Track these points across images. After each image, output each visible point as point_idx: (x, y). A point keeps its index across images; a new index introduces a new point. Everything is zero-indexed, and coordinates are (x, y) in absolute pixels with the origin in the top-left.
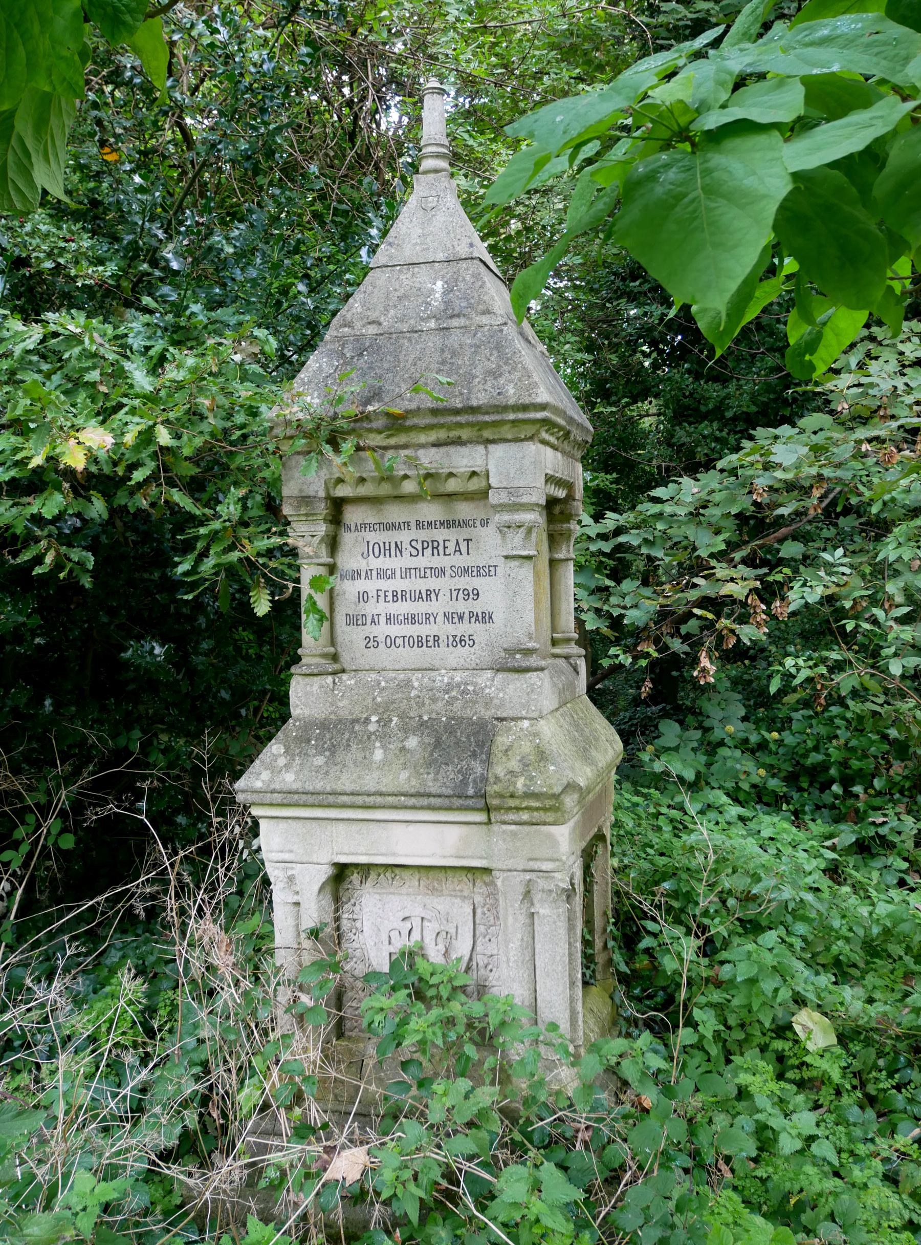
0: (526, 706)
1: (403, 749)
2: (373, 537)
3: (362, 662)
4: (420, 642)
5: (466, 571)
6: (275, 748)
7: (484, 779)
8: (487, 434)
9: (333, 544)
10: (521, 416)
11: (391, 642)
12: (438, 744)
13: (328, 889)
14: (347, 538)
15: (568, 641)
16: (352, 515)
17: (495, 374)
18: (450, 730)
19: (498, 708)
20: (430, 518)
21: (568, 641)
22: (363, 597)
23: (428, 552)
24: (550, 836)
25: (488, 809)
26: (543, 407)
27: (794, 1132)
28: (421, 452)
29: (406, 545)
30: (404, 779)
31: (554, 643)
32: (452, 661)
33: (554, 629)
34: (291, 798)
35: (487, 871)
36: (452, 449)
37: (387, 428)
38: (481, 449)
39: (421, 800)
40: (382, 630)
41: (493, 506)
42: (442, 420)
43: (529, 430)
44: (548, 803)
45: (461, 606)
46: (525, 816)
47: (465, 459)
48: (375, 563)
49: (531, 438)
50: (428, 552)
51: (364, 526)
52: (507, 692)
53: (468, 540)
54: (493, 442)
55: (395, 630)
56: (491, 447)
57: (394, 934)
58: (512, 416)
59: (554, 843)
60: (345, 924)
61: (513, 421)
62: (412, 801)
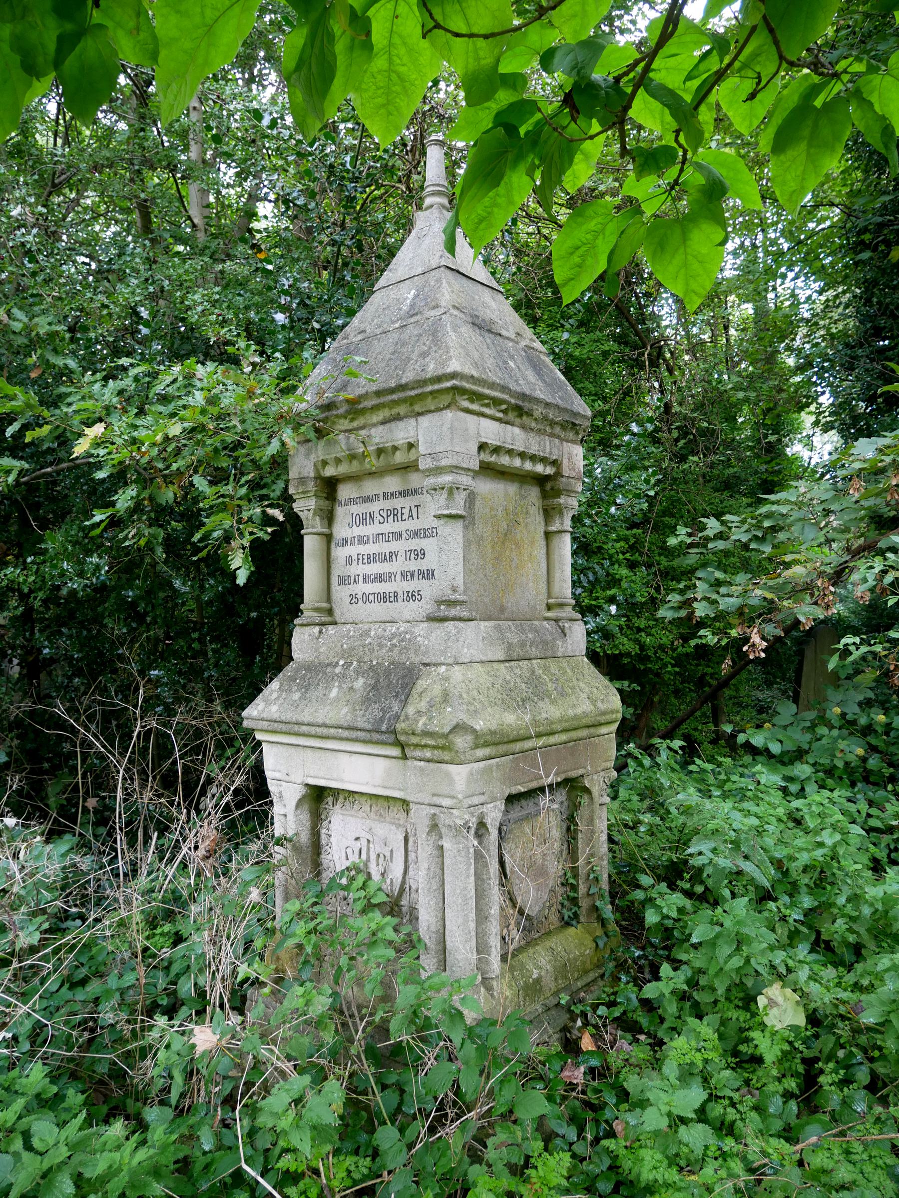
0: (443, 653)
1: (351, 688)
2: (356, 509)
3: (348, 616)
4: (384, 598)
5: (416, 534)
6: (275, 685)
7: (397, 717)
8: (417, 408)
9: (329, 518)
10: (437, 387)
11: (366, 599)
12: (374, 687)
13: (306, 806)
14: (340, 512)
15: (561, 605)
16: (345, 492)
17: (424, 355)
18: (388, 673)
19: (424, 654)
20: (392, 490)
21: (561, 605)
22: (349, 561)
23: (391, 518)
24: (448, 774)
25: (402, 746)
26: (454, 375)
27: (665, 1109)
28: (373, 430)
29: (376, 515)
30: (342, 714)
31: (549, 607)
32: (407, 615)
33: (549, 596)
34: (290, 728)
35: (405, 803)
36: (393, 425)
37: (348, 412)
38: (412, 421)
39: (351, 733)
40: (363, 588)
41: (423, 472)
42: (383, 400)
43: (446, 399)
44: (441, 742)
45: (413, 565)
46: (428, 754)
47: (402, 432)
48: (358, 531)
49: (448, 407)
50: (391, 518)
51: (351, 501)
52: (432, 639)
53: (417, 506)
54: (419, 414)
55: (369, 588)
56: (420, 419)
57: (349, 851)
58: (429, 388)
59: (451, 781)
60: (324, 839)
61: (431, 393)
62: (346, 734)
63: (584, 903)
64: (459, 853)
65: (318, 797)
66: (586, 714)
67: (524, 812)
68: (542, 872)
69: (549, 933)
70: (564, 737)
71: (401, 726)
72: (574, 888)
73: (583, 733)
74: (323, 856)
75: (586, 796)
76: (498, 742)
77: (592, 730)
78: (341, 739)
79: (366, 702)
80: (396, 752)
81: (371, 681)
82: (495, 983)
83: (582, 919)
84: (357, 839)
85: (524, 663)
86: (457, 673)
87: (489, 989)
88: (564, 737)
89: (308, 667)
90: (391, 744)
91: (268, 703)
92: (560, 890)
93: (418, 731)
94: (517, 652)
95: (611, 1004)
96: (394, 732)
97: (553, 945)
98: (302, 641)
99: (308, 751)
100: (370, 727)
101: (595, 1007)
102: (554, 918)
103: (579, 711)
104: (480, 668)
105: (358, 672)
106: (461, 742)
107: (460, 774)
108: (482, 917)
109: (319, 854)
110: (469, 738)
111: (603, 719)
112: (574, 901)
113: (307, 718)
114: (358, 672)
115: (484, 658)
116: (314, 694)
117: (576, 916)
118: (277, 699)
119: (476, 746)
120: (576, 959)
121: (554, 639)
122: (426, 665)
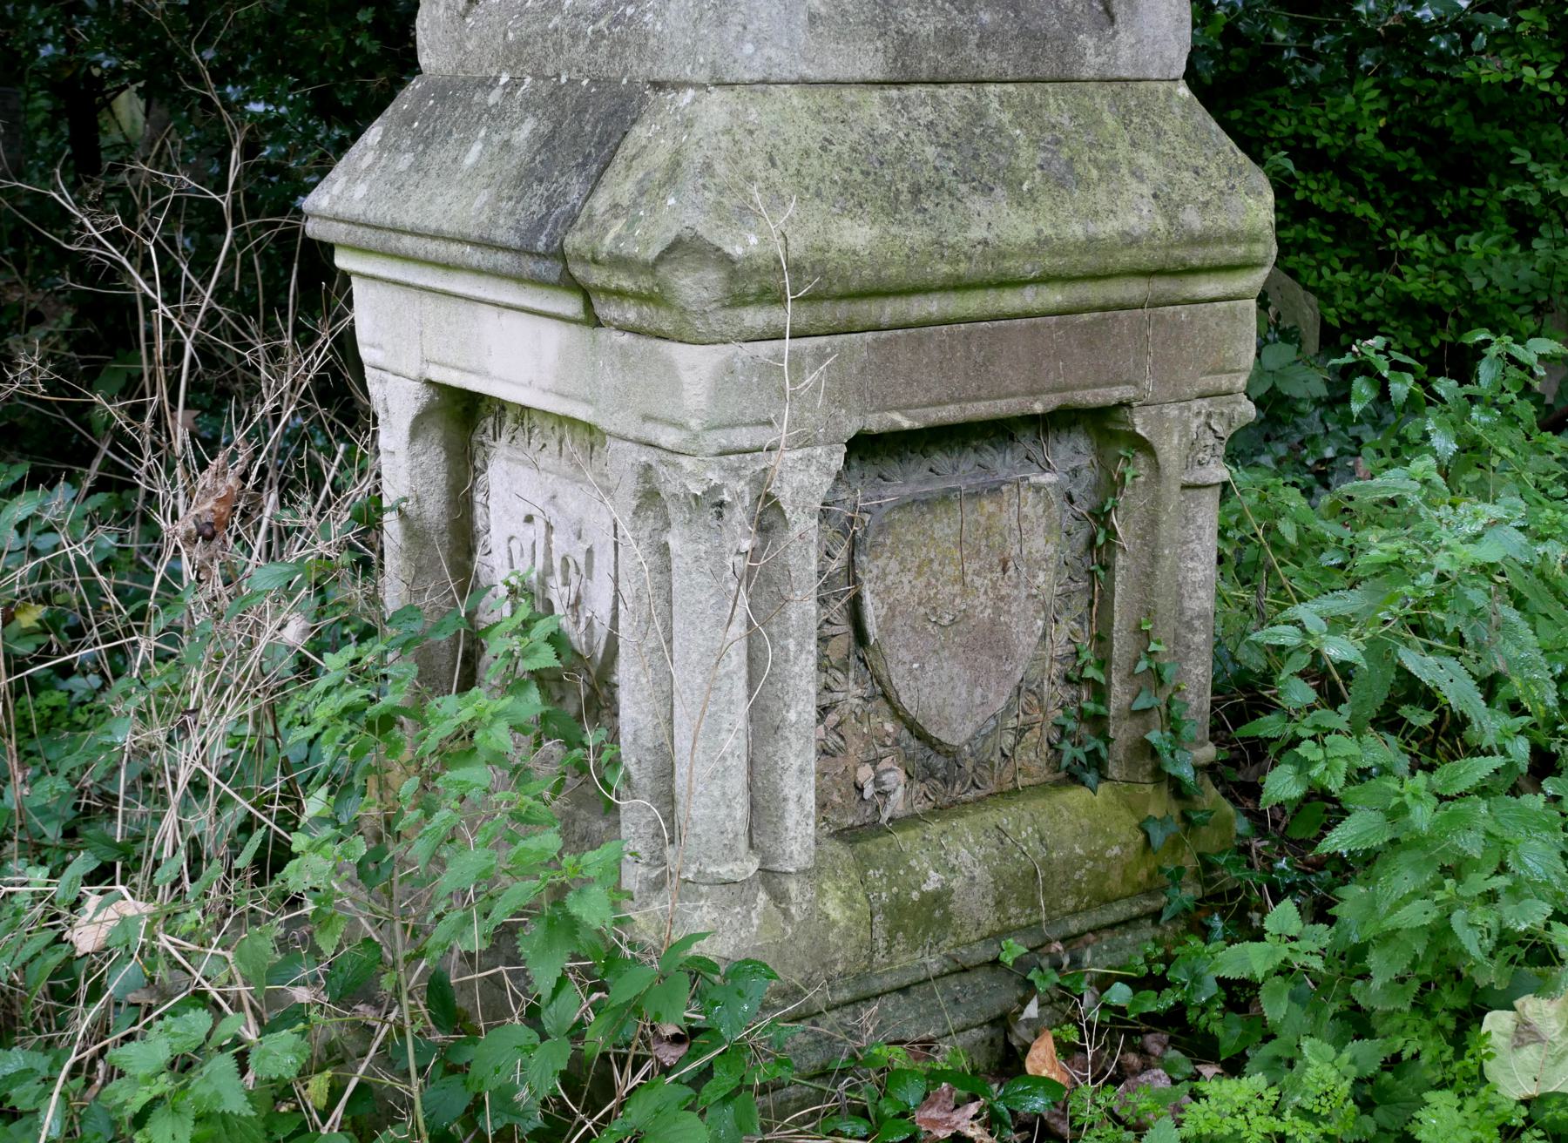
13: (436, 434)
24: (669, 366)
25: (586, 293)
34: (385, 239)
44: (645, 282)
62: (475, 257)
63: (1122, 733)
64: (706, 562)
65: (463, 416)
66: (1130, 240)
67: (938, 486)
68: (990, 641)
69: (1011, 794)
70: (1055, 296)
71: (575, 241)
72: (1100, 692)
73: (1135, 289)
74: (478, 557)
75: (1142, 460)
76: (834, 297)
77: (1162, 286)
78: (478, 271)
79: (528, 176)
80: (571, 305)
81: (546, 128)
82: (793, 887)
83: (1114, 771)
84: (529, 519)
85: (953, 95)
86: (715, 109)
87: (779, 897)
88: (1055, 296)
89: (445, 91)
90: (556, 285)
91: (352, 181)
92: (1057, 693)
93: (602, 256)
94: (932, 59)
95: (1158, 983)
96: (560, 255)
97: (1007, 822)
98: (434, 22)
99: (428, 299)
100: (515, 241)
101: (1103, 983)
102: (1033, 760)
103: (1107, 228)
104: (795, 97)
105: (527, 105)
106: (693, 286)
107: (695, 365)
108: (764, 724)
109: (470, 552)
110: (713, 276)
111: (1196, 257)
112: (1098, 722)
113: (409, 219)
114: (527, 105)
115: (811, 73)
116: (440, 155)
117: (1096, 762)
118: (370, 168)
119: (738, 300)
120: (1071, 864)
121: (1072, 28)
122: (658, 86)
